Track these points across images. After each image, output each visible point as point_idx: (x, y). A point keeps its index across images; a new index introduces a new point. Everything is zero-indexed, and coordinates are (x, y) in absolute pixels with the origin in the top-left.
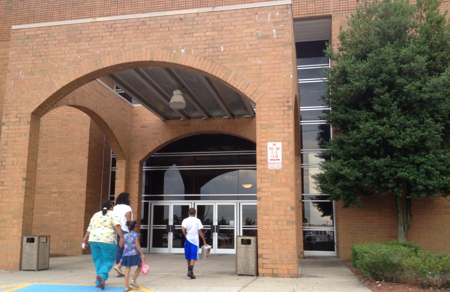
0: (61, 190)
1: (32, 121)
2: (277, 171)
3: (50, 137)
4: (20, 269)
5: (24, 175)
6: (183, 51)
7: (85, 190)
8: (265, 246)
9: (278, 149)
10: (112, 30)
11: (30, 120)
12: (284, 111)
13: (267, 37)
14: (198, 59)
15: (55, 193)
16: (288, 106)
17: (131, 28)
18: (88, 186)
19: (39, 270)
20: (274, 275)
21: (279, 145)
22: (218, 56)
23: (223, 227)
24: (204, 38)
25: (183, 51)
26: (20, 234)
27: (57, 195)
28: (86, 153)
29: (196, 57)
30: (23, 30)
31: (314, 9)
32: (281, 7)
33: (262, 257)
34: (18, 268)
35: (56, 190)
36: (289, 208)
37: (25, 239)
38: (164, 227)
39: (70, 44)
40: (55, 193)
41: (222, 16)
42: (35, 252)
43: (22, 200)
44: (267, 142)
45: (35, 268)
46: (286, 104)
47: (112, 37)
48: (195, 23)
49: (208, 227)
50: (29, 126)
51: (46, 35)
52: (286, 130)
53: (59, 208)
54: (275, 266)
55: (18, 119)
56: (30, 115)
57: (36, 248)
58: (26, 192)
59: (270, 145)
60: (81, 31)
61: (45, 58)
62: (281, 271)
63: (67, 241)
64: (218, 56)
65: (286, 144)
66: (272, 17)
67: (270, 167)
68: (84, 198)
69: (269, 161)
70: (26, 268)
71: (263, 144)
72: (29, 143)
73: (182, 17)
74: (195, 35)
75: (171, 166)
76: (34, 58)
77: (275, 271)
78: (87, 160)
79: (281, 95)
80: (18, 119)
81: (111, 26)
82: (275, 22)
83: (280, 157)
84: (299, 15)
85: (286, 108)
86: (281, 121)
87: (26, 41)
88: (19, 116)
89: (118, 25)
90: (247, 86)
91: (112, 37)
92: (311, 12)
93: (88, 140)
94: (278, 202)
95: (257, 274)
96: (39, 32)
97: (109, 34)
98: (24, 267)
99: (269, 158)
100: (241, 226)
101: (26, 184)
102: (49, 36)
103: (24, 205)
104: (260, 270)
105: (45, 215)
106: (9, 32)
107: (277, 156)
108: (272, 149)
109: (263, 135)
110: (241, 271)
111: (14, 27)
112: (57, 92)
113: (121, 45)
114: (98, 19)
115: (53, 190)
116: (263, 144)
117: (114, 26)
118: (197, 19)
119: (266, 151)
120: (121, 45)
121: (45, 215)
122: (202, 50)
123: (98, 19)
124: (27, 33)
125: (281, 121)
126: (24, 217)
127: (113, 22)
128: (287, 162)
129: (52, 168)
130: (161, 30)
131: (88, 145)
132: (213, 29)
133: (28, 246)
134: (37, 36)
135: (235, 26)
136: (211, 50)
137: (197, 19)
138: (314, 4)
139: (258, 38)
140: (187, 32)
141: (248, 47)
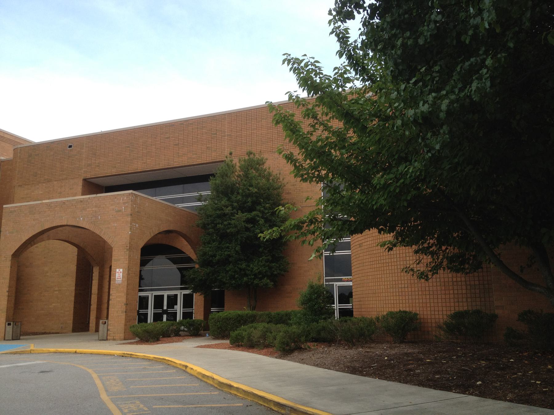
0: (60, 289)
1: (12, 260)
2: (119, 284)
3: (54, 252)
4: (4, 340)
5: (7, 289)
6: (81, 219)
7: (74, 288)
8: (111, 325)
9: (121, 272)
10: (49, 207)
11: (11, 259)
12: (125, 252)
13: (120, 211)
14: (88, 223)
15: (56, 291)
16: (127, 249)
17: (58, 206)
18: (77, 285)
19: (13, 339)
20: (114, 340)
21: (121, 270)
22: (97, 221)
23: (170, 310)
24: (91, 212)
25: (81, 219)
26: (5, 321)
27: (57, 292)
28: (75, 263)
29: (87, 222)
30: (8, 208)
31: (215, 156)
32: (127, 194)
33: (109, 330)
34: (3, 339)
35: (58, 289)
36: (123, 304)
37: (7, 323)
38: (160, 311)
39: (30, 216)
40: (56, 291)
41: (100, 200)
42: (11, 330)
43: (6, 303)
44: (116, 269)
45: (11, 339)
46: (126, 248)
47: (49, 212)
48: (88, 203)
49: (160, 311)
50: (10, 262)
51: (19, 211)
52: (125, 262)
53: (59, 301)
54: (115, 335)
55: (5, 259)
56: (11, 256)
57: (11, 328)
58: (8, 298)
59: (117, 270)
60: (35, 208)
61: (18, 223)
62: (117, 338)
63: (63, 324)
64: (97, 221)
65: (124, 269)
66: (123, 200)
67: (116, 282)
68: (73, 294)
69: (116, 279)
70: (7, 339)
71: (114, 270)
72: (10, 272)
73: (82, 200)
74: (87, 210)
75: (145, 266)
76: (13, 224)
77: (115, 338)
78: (76, 267)
79: (124, 243)
80: (5, 259)
81: (49, 205)
82: (124, 203)
83: (121, 277)
84: (206, 160)
85: (126, 250)
86: (123, 257)
87: (10, 214)
88: (6, 257)
89: (52, 205)
90: (109, 238)
91: (49, 212)
92: (214, 159)
93: (76, 254)
94: (119, 301)
95: (107, 340)
96: (16, 209)
97: (48, 210)
98: (6, 339)
99: (117, 277)
100: (182, 309)
101: (8, 294)
102: (21, 211)
103: (7, 305)
104: (108, 337)
105: (50, 306)
106: (3, 208)
107: (120, 277)
108: (118, 272)
109: (115, 265)
110: (101, 338)
111: (4, 206)
112: (24, 243)
113: (53, 216)
114: (44, 201)
115: (56, 289)
116: (114, 270)
117: (51, 205)
118: (89, 201)
119: (116, 274)
120: (53, 216)
121: (50, 306)
122: (90, 218)
123: (44, 201)
124: (11, 210)
125: (123, 257)
126: (7, 312)
127: (50, 203)
128: (124, 279)
129: (55, 274)
130: (72, 207)
131: (76, 257)
132: (96, 207)
133: (7, 327)
134: (15, 211)
135: (106, 205)
136: (94, 218)
137: (89, 201)
138: (215, 153)
139: (116, 212)
140: (84, 208)
141: (111, 216)
